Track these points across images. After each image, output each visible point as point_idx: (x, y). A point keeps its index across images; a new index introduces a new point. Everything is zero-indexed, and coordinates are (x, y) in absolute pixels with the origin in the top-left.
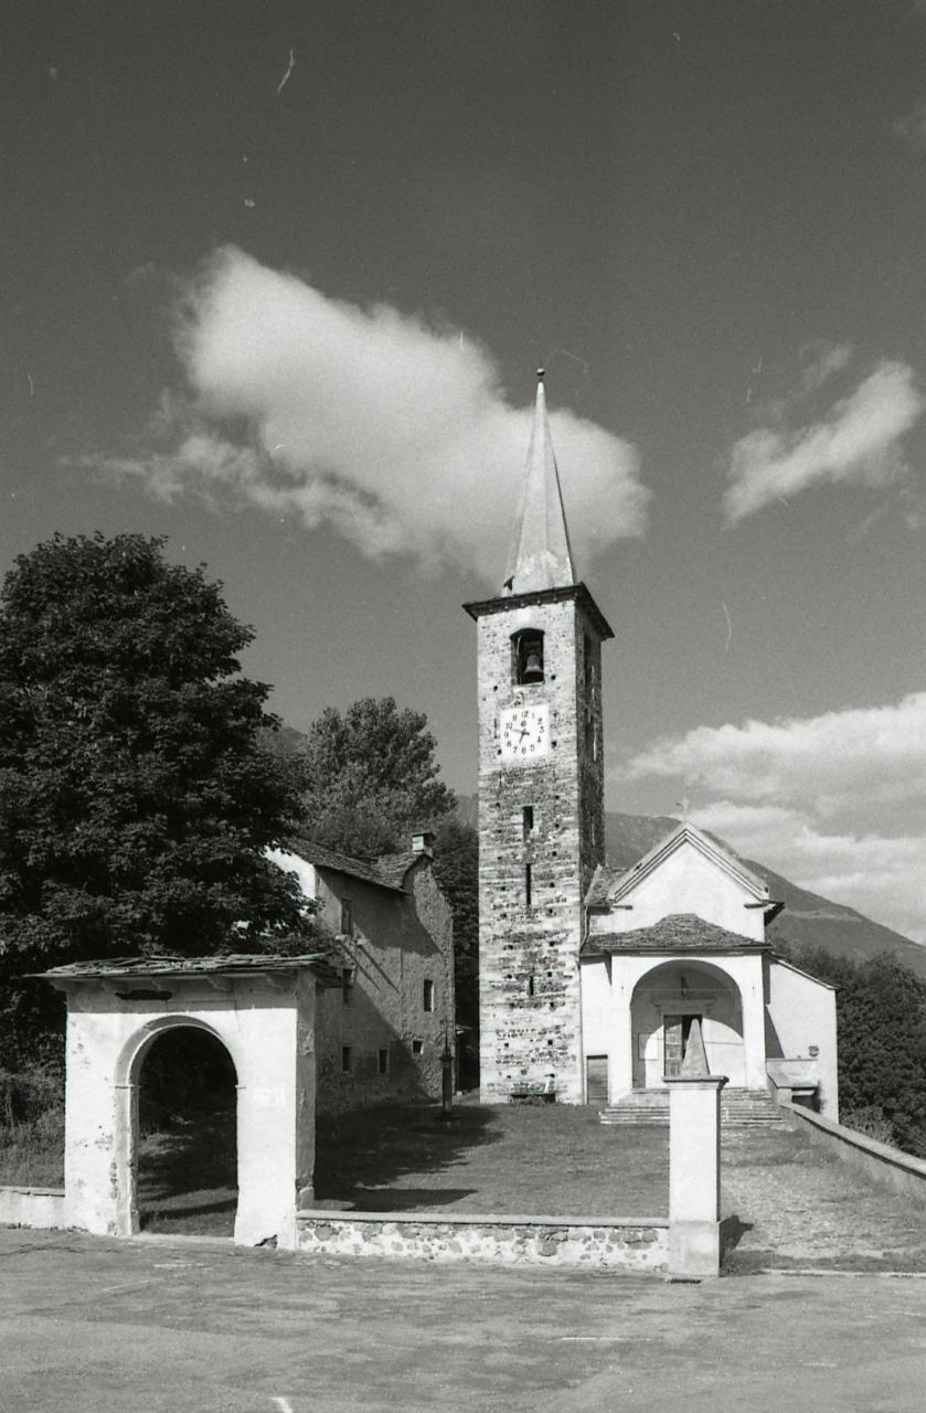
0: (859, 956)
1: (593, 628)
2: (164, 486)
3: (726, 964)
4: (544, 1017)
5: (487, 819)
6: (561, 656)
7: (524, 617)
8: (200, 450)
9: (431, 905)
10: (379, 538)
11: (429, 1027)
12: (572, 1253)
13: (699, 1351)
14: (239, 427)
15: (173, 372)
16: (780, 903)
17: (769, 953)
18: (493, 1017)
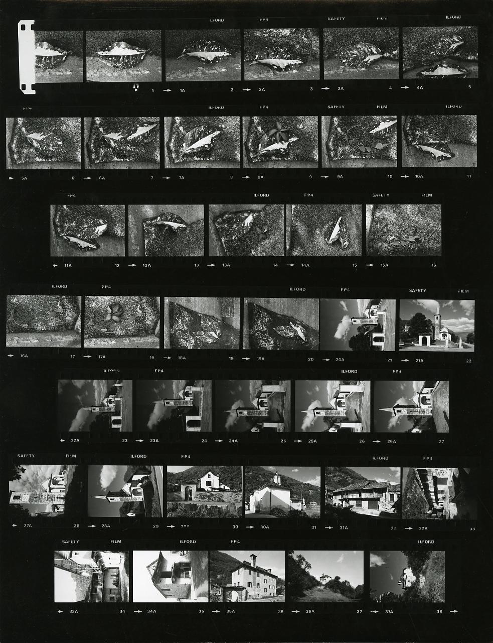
0: (370, 304)
1: (353, 318)
2: (346, 340)
3: (421, 397)
4: (425, 411)
5: (363, 323)
6: (355, 320)
7: (396, 412)
8: (344, 338)
9: (368, 326)
10: (349, 329)
11: (374, 327)
12: (385, 319)
13: (390, 312)
14: (343, 336)
15: (340, 339)
16: (367, 308)
17: (370, 309)
18: (373, 323)
